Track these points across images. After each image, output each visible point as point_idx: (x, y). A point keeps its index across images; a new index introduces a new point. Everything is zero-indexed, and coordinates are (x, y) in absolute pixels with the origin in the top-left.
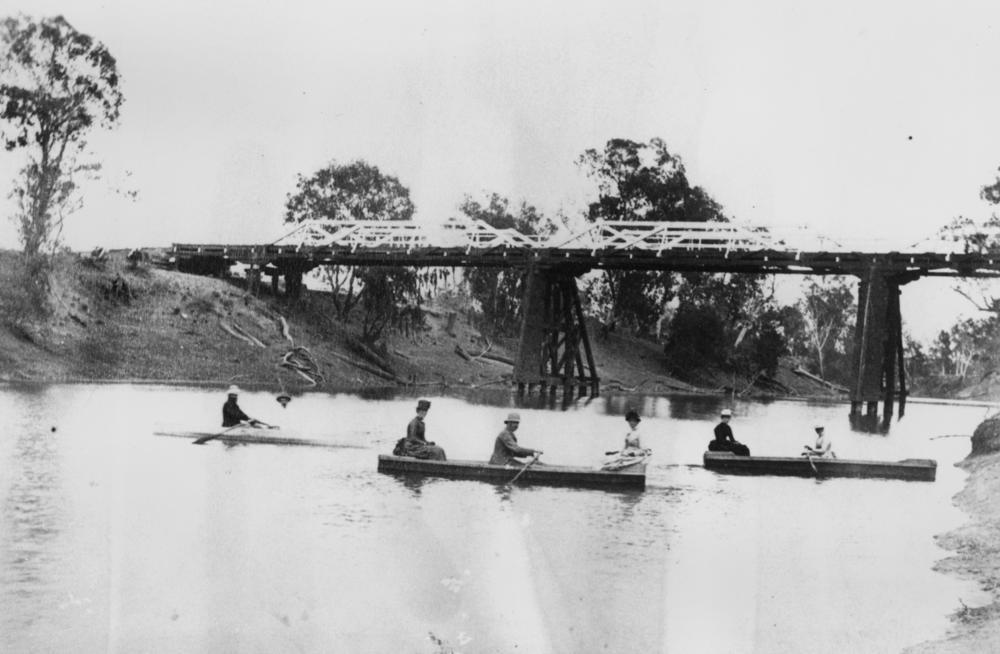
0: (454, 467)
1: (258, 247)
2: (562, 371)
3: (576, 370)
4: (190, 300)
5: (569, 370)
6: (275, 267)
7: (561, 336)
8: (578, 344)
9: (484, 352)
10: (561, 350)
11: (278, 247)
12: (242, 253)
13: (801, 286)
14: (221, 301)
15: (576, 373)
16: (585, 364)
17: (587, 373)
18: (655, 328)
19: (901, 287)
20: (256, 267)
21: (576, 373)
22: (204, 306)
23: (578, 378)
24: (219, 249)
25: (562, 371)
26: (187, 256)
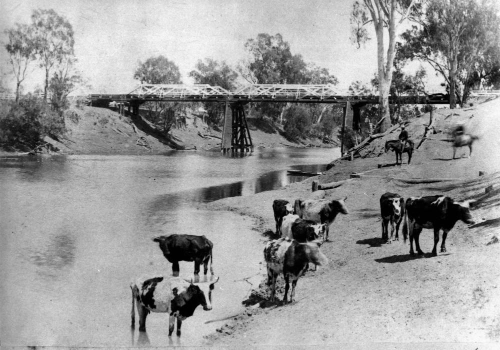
0: (383, 234)
1: (123, 95)
2: (239, 143)
3: (245, 141)
4: (100, 119)
5: (242, 142)
6: (414, 240)
7: (239, 128)
8: (388, 223)
9: (209, 134)
10: (239, 134)
11: (131, 95)
12: (117, 98)
13: (348, 92)
14: (111, 119)
15: (245, 143)
16: (248, 140)
17: (249, 143)
18: (280, 118)
19: (409, 254)
20: (122, 104)
21: (245, 143)
22: (105, 121)
23: (245, 145)
24: (108, 96)
25: (239, 143)
26: (96, 99)
